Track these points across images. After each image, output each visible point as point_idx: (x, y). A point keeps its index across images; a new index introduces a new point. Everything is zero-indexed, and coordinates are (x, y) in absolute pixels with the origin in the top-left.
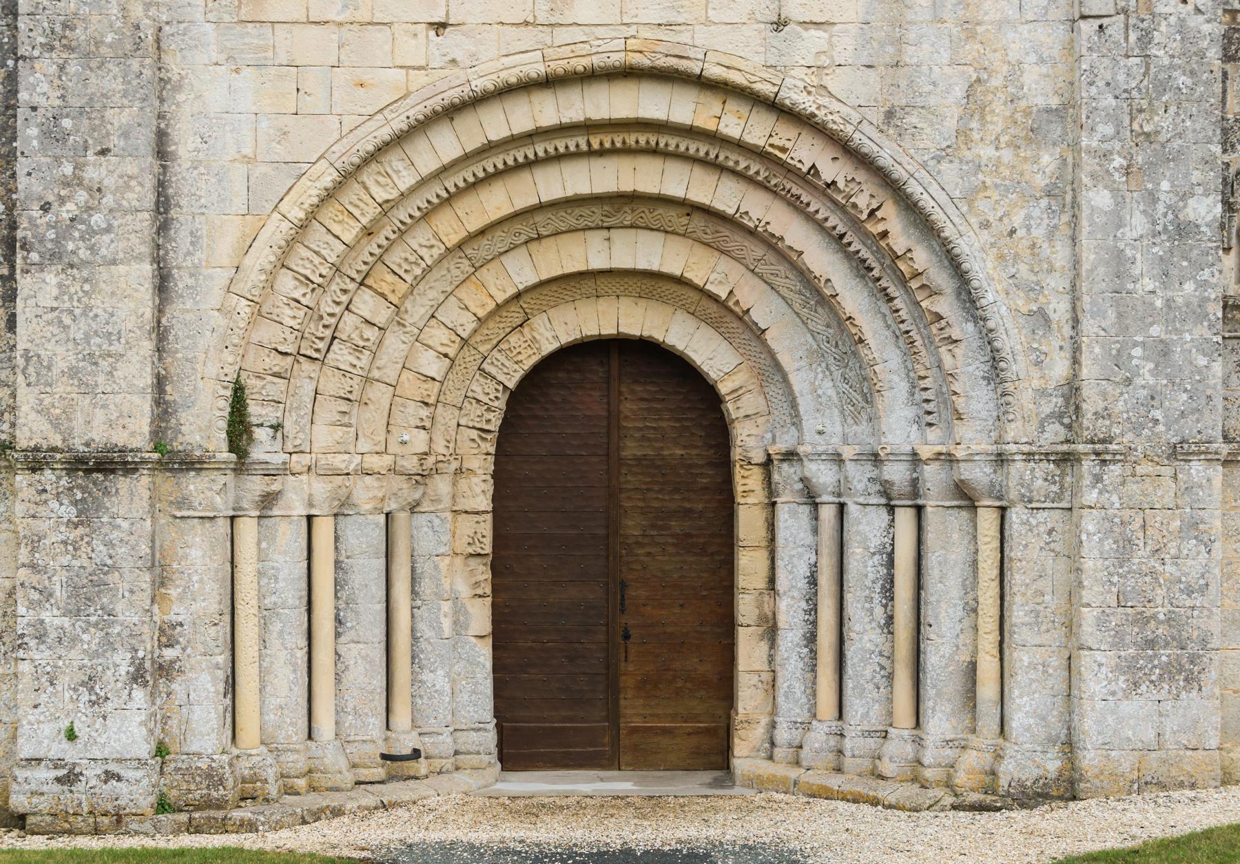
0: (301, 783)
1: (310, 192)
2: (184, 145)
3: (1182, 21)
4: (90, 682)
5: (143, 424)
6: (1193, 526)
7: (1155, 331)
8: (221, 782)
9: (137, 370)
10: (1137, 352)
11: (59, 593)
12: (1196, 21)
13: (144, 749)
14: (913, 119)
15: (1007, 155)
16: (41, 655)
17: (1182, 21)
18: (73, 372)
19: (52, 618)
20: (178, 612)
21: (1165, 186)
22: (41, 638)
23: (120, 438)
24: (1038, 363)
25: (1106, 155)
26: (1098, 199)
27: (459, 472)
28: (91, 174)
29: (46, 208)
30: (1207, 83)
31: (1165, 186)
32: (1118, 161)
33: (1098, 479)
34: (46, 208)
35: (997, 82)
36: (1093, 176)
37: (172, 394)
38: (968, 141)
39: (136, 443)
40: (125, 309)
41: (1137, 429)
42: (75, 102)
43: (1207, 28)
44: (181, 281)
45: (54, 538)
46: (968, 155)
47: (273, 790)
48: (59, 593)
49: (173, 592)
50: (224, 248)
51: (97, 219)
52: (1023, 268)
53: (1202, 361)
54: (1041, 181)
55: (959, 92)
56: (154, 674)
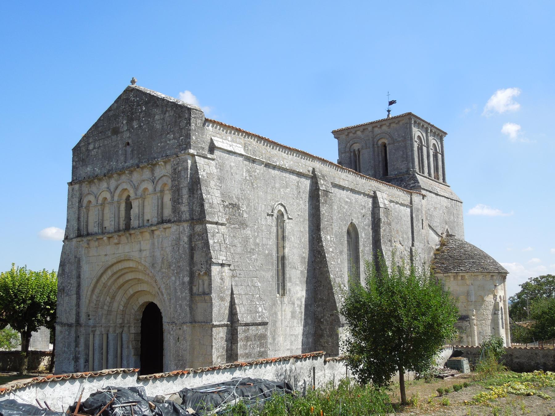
2: (82, 276)
5: (74, 320)
9: (74, 312)
15: (166, 271)
19: (66, 350)
20: (80, 349)
25: (174, 270)
27: (129, 327)
32: (176, 271)
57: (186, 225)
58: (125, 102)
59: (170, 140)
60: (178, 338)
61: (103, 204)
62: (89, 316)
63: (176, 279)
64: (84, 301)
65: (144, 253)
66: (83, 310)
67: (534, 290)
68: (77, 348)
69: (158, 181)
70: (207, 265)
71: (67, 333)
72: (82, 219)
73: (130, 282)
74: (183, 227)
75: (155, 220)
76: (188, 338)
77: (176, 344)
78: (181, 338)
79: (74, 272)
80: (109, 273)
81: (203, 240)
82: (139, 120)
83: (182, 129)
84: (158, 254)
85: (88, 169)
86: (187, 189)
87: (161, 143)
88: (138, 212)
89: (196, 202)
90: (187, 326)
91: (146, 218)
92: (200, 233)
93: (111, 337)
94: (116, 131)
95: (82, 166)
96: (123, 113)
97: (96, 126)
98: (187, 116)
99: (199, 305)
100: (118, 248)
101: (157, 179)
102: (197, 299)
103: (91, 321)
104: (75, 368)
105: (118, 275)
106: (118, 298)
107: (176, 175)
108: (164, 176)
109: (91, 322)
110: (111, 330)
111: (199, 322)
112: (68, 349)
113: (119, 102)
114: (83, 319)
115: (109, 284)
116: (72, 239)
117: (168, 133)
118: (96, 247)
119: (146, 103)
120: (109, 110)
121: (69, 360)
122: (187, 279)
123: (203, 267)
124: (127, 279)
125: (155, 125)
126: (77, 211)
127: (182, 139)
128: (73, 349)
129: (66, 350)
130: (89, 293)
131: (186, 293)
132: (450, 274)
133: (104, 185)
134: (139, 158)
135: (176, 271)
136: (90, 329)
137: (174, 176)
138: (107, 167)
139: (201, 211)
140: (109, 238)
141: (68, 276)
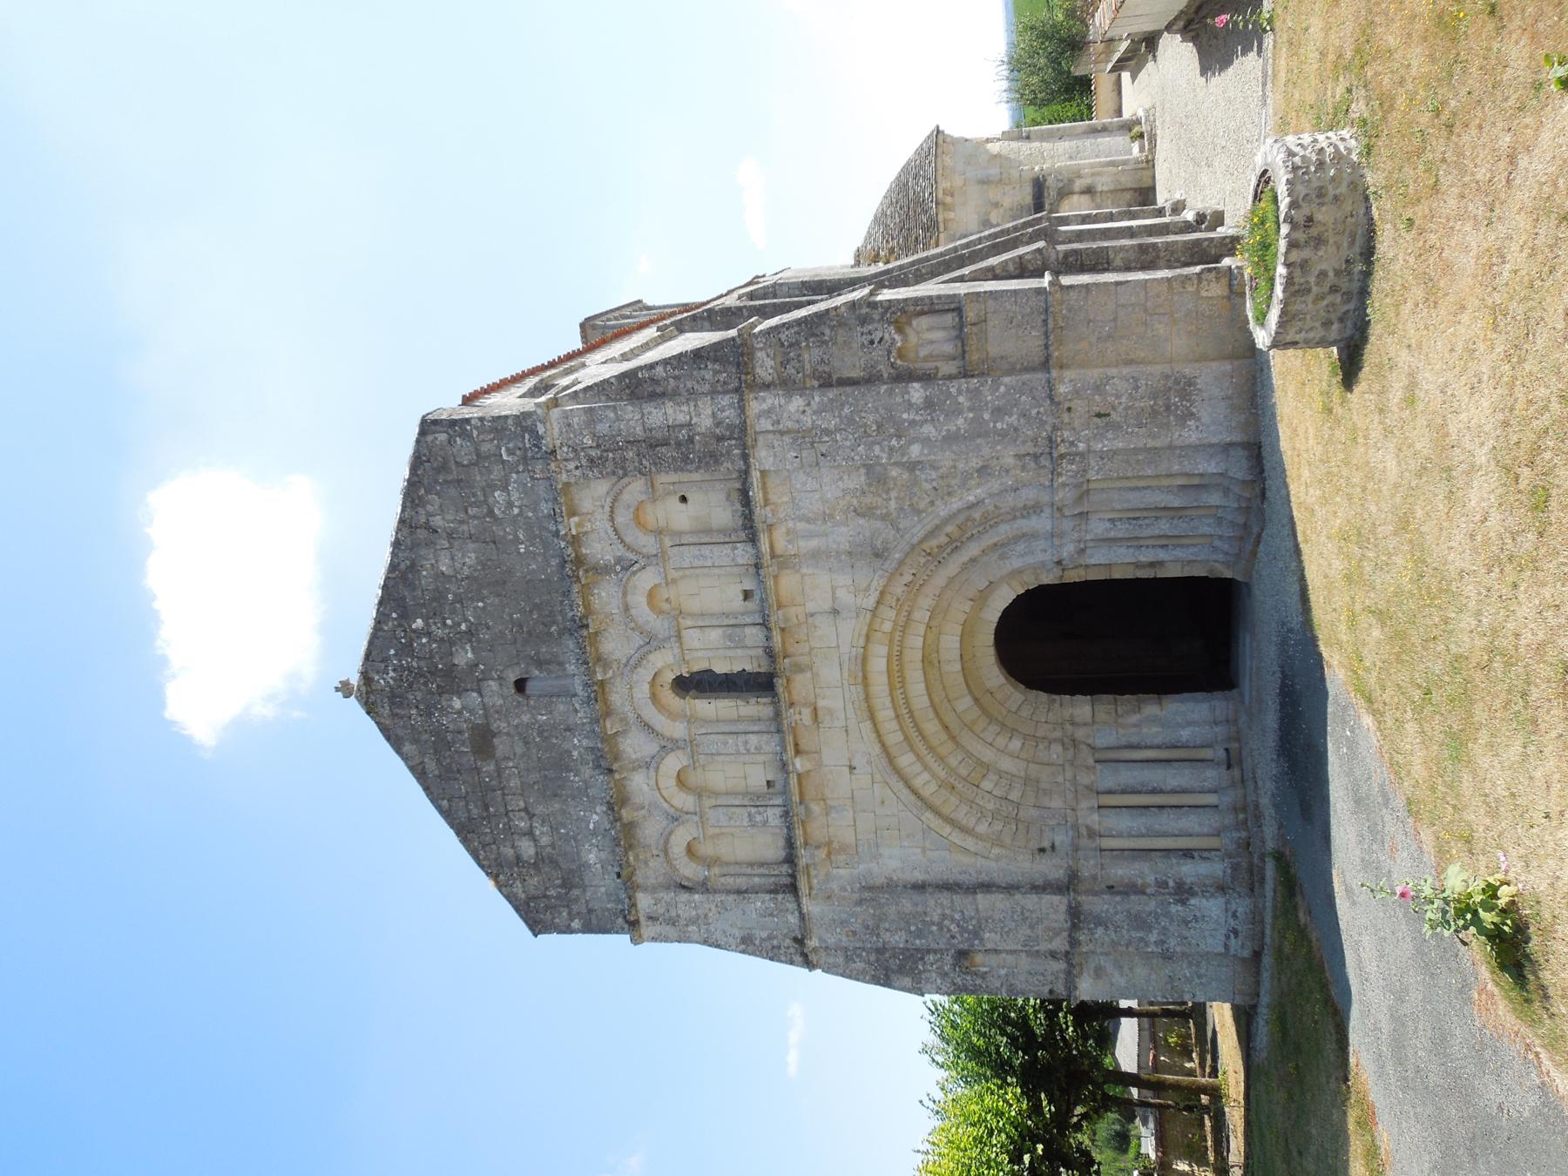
0: (1241, 816)
1: (935, 822)
2: (919, 876)
3: (814, 413)
4: (1186, 923)
5: (1056, 899)
6: (1098, 389)
7: (986, 416)
8: (1238, 864)
9: (1030, 901)
10: (999, 425)
11: (1140, 934)
12: (814, 405)
13: (1221, 901)
14: (878, 543)
15: (893, 494)
16: (1172, 942)
17: (814, 413)
18: (1032, 927)
19: (1153, 937)
20: (1151, 879)
21: (905, 416)
22: (1163, 942)
23: (1063, 908)
24: (1007, 471)
25: (891, 449)
26: (915, 450)
27: (1073, 724)
28: (936, 919)
29: (953, 937)
30: (847, 396)
31: (905, 416)
32: (894, 442)
33: (1072, 444)
34: (953, 937)
35: (855, 502)
36: (903, 455)
37: (1040, 882)
38: (888, 515)
39: (1065, 900)
40: (999, 905)
41: (1043, 423)
42: (903, 924)
43: (817, 399)
44: (984, 878)
45: (1113, 936)
46: (895, 515)
47: (1244, 834)
48: (1140, 934)
49: (1140, 881)
50: (966, 860)
51: (957, 916)
52: (953, 482)
53: (1002, 389)
54: (906, 476)
55: (861, 521)
56: (1183, 892)
57: (754, 407)
58: (401, 705)
59: (510, 505)
60: (1099, 415)
61: (699, 793)
62: (1042, 850)
64: (995, 864)
65: (844, 596)
66: (1026, 866)
68: (1148, 891)
69: (629, 548)
70: (872, 320)
71: (1100, 931)
72: (742, 882)
73: (937, 700)
74: (759, 416)
75: (743, 554)
76: (1094, 374)
77: (1116, 427)
78: (1098, 403)
79: (907, 905)
80: (906, 760)
81: (798, 343)
82: (452, 643)
83: (478, 455)
84: (842, 536)
85: (592, 858)
86: (649, 408)
87: (517, 541)
88: (720, 631)
89: (689, 384)
90: (1061, 381)
91: (738, 603)
92: (779, 359)
93: (1108, 782)
94: (483, 740)
95: (584, 888)
96: (430, 714)
97: (465, 831)
98: (443, 437)
99: (994, 350)
100: (830, 712)
101: (620, 551)
102: (975, 357)
103: (1058, 840)
104: (1212, 896)
105: (913, 734)
106: (987, 755)
107: (611, 458)
108: (612, 519)
109: (1062, 838)
110: (1085, 779)
111: (1046, 346)
112: (1150, 929)
113: (400, 732)
114: (1053, 869)
115: (942, 774)
116: (802, 916)
117: (491, 513)
118: (828, 811)
119: (406, 616)
120: (420, 773)
121: (1186, 923)
122: (917, 392)
123: (877, 336)
124: (925, 701)
125: (466, 571)
126: (718, 898)
127: (510, 452)
128: (1152, 905)
129: (1153, 937)
130: (969, 843)
131: (960, 392)
132: (940, 218)
133: (639, 784)
134: (561, 633)
136: (1084, 842)
137: (610, 466)
138: (587, 771)
139: (715, 360)
140: (798, 752)
141: (919, 934)
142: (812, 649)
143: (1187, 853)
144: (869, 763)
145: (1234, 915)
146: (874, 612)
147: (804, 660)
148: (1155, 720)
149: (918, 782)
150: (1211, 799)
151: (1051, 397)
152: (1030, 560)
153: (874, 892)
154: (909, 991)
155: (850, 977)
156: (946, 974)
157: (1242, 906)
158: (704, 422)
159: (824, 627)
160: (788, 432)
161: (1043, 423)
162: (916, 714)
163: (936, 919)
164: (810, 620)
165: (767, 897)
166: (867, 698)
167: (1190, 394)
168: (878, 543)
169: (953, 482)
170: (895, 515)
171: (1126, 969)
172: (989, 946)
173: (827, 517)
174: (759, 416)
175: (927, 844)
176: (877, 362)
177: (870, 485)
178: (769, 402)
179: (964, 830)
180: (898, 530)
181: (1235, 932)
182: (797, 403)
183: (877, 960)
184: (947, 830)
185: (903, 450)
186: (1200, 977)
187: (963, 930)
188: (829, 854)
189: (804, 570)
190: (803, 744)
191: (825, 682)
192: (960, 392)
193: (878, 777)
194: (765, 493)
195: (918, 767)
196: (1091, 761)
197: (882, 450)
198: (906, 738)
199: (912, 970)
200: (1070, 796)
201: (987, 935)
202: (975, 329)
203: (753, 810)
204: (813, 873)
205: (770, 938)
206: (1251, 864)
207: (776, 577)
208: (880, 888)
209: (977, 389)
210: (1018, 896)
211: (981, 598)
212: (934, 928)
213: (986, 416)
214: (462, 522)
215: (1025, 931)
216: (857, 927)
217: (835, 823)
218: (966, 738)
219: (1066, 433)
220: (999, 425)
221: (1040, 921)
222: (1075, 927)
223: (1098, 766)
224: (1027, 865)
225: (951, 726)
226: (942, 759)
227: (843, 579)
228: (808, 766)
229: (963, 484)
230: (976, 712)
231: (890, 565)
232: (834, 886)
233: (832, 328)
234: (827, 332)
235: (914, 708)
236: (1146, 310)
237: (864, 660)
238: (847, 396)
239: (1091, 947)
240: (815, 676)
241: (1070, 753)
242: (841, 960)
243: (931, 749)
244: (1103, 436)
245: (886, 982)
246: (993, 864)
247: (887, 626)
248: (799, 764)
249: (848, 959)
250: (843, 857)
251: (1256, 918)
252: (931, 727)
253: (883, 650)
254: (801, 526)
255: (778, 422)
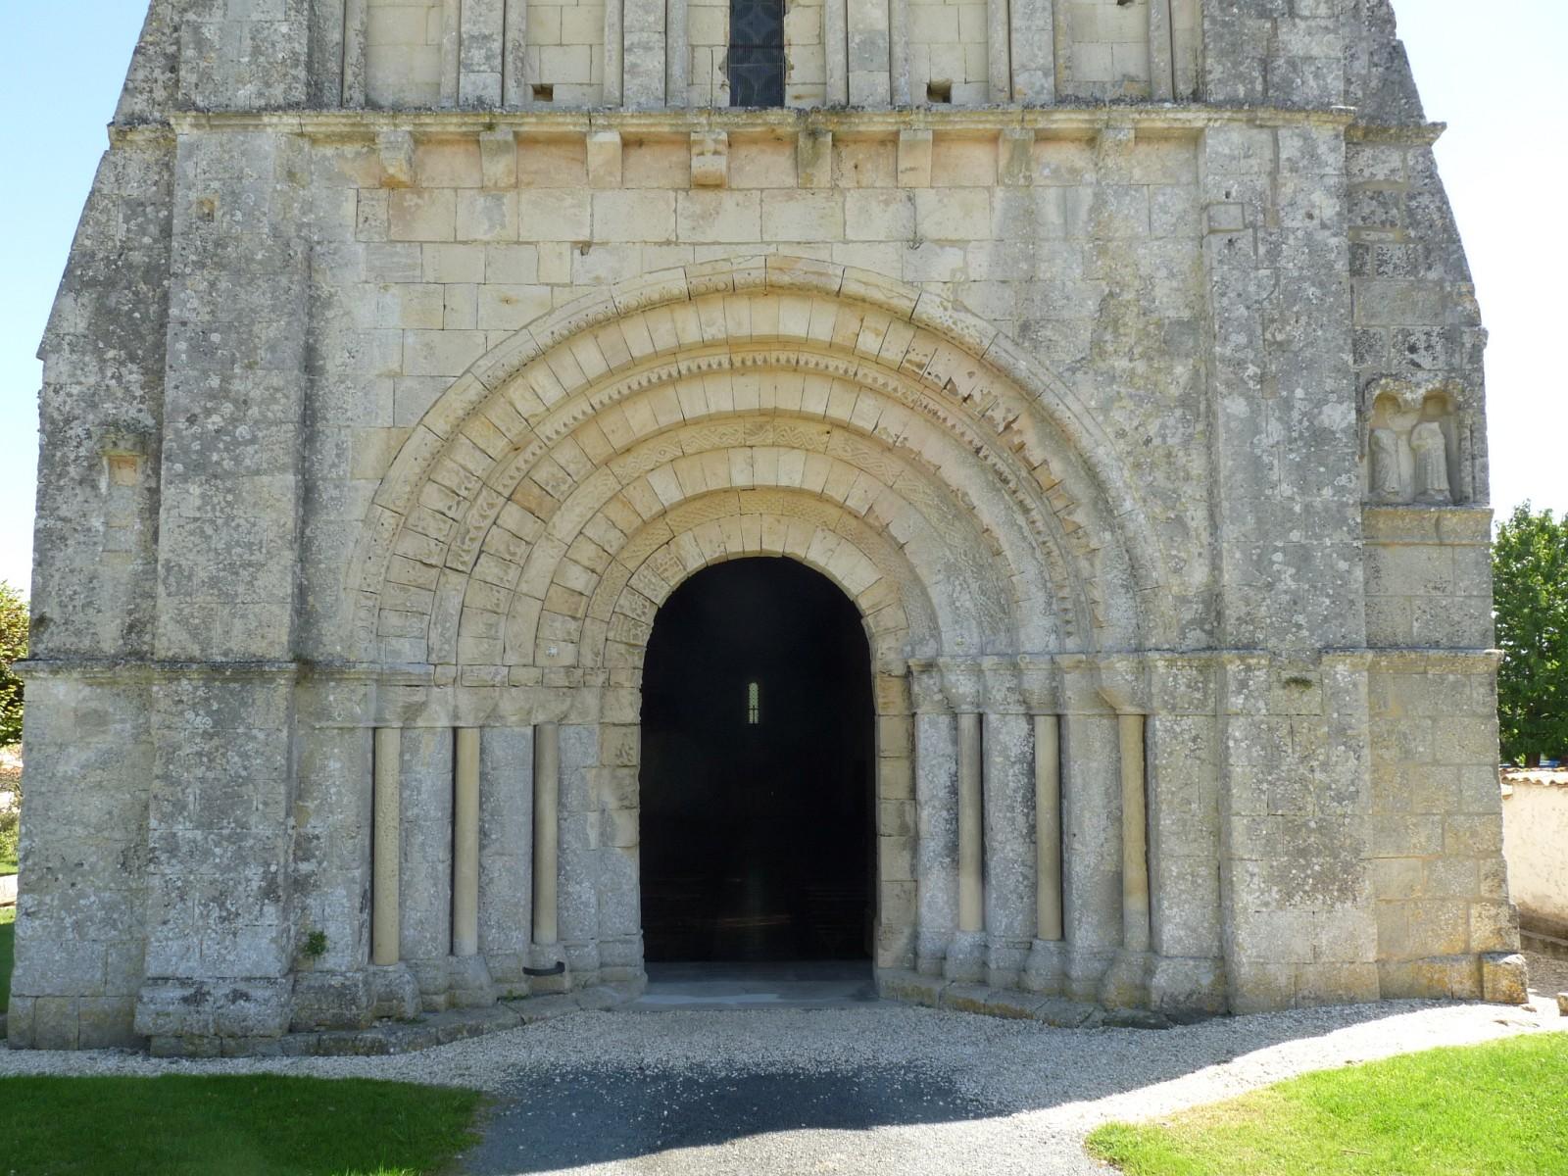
2: (334, 361)
3: (1309, 235)
4: (220, 899)
7: (1295, 536)
9: (277, 579)
10: (1278, 557)
11: (193, 806)
12: (1322, 236)
14: (1047, 333)
15: (1141, 367)
16: (172, 870)
18: (213, 582)
19: (184, 831)
20: (315, 826)
23: (258, 647)
25: (1241, 364)
26: (1235, 406)
28: (237, 386)
29: (192, 420)
30: (1337, 294)
31: (1299, 393)
32: (1252, 370)
33: (1243, 684)
36: (1228, 384)
38: (1102, 354)
39: (276, 652)
40: (266, 519)
42: (225, 318)
43: (1333, 241)
44: (327, 492)
46: (1103, 366)
48: (193, 806)
49: (311, 805)
50: (371, 457)
51: (242, 431)
52: (1160, 475)
53: (1343, 565)
54: (1174, 391)
55: (1092, 305)
56: (289, 889)
63: (1255, 410)
67: (1531, 530)
71: (203, 722)
74: (1306, 138)
80: (589, 357)
84: (1064, 268)
88: (883, 25)
106: (565, 524)
112: (205, 825)
114: (343, 631)
115: (547, 430)
121: (220, 899)
122: (1339, 416)
123: (1425, 360)
129: (184, 831)
130: (408, 467)
131: (1341, 490)
135: (1252, 370)
136: (400, 696)
139: (1385, 81)
141: (202, 349)
142: (843, 192)
143: (370, 899)
144: (598, 281)
145: (238, 995)
146: (910, 320)
147: (823, 175)
148: (606, 837)
149: (540, 378)
150: (468, 942)
151: (1328, 648)
152: (944, 617)
153: (303, 268)
154: (51, 327)
155: (90, 204)
156: (93, 406)
157: (264, 1011)
158: (1296, 40)
159: (884, 220)
160: (1275, 185)
161: (1281, 633)
162: (670, 391)
163: (237, 386)
164: (902, 195)
165: (301, 47)
166: (733, 290)
167: (1326, 890)
168: (1047, 333)
169: (1160, 475)
170: (1103, 366)
171: (96, 776)
172: (168, 493)
173: (1101, 245)
174: (1306, 138)
175: (408, 383)
176: (1378, 356)
177: (1159, 326)
178: (1331, 159)
179: (435, 459)
180: (1073, 370)
181: (197, 998)
182: (1328, 207)
183: (130, 266)
184: (441, 425)
185: (1235, 385)
186: (78, 926)
187: (209, 442)
188: (392, 184)
189: (1000, 193)
190: (643, 158)
191: (768, 213)
192: (1341, 490)
193: (562, 296)
194: (1164, 137)
195: (572, 379)
196: (539, 717)
197: (1237, 348)
198: (634, 362)
199: (107, 336)
200: (485, 674)
201: (195, 490)
202: (1429, 526)
203: (497, 46)
204: (349, 149)
205: (200, 44)
206: (352, 1025)
207: (994, 139)
208: (309, 282)
209: (1344, 521)
210: (289, 556)
211: (865, 529)
212: (215, 382)
213: (1295, 536)
214: (243, 143)
215: (204, 568)
216: (222, 222)
217: (458, 201)
218: (601, 486)
219: (1261, 675)
220: (1278, 557)
221: (228, 599)
222: (214, 670)
223: (529, 731)
224: (355, 580)
225: (630, 459)
226: (574, 434)
227: (979, 263)
228: (595, 159)
229: (1153, 492)
230: (647, 508)
231: (1004, 352)
232: (317, 189)
233: (1440, 283)
234: (1432, 275)
235: (683, 389)
236: (1449, 814)
237: (801, 291)
238: (1337, 294)
239: (164, 704)
240: (789, 194)
241: (560, 680)
242: (133, 190)
243: (596, 414)
244: (1255, 740)
245: (73, 281)
246: (358, 511)
247: (869, 343)
248: (605, 141)
249: (135, 207)
250: (382, 212)
251: (233, 1041)
252: (640, 418)
253: (822, 331)
254: (1086, 195)
255: (1294, 170)
